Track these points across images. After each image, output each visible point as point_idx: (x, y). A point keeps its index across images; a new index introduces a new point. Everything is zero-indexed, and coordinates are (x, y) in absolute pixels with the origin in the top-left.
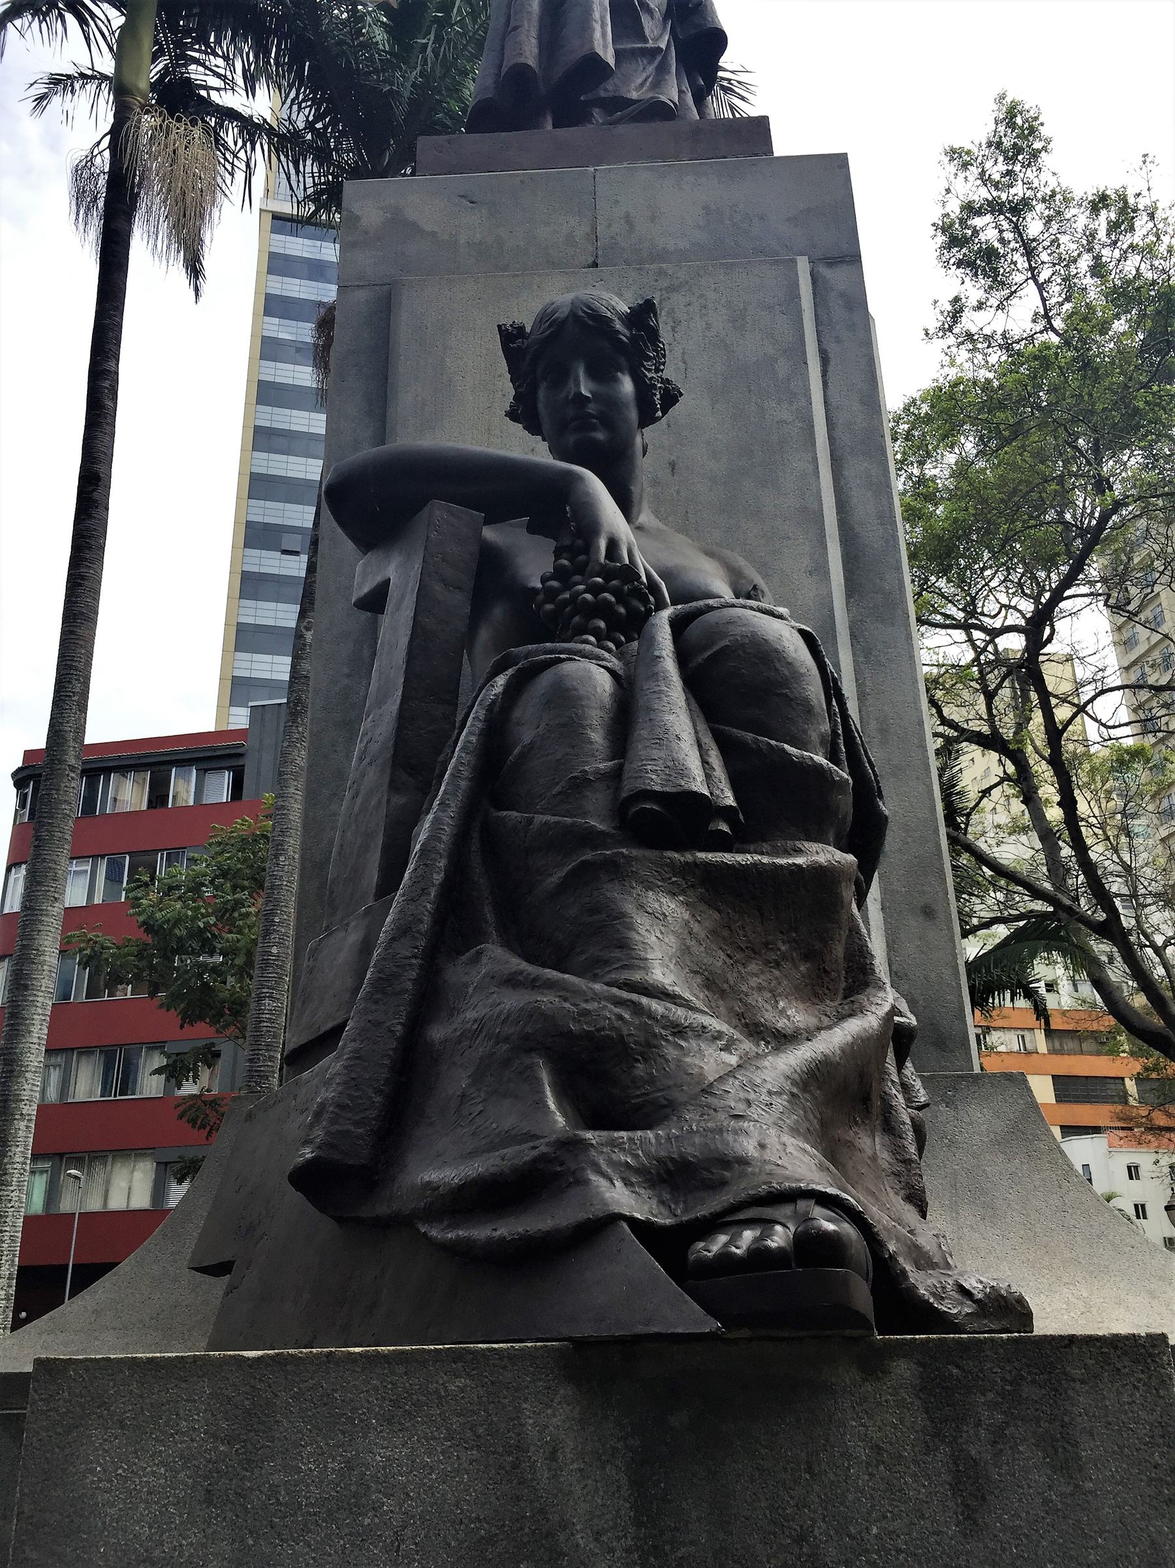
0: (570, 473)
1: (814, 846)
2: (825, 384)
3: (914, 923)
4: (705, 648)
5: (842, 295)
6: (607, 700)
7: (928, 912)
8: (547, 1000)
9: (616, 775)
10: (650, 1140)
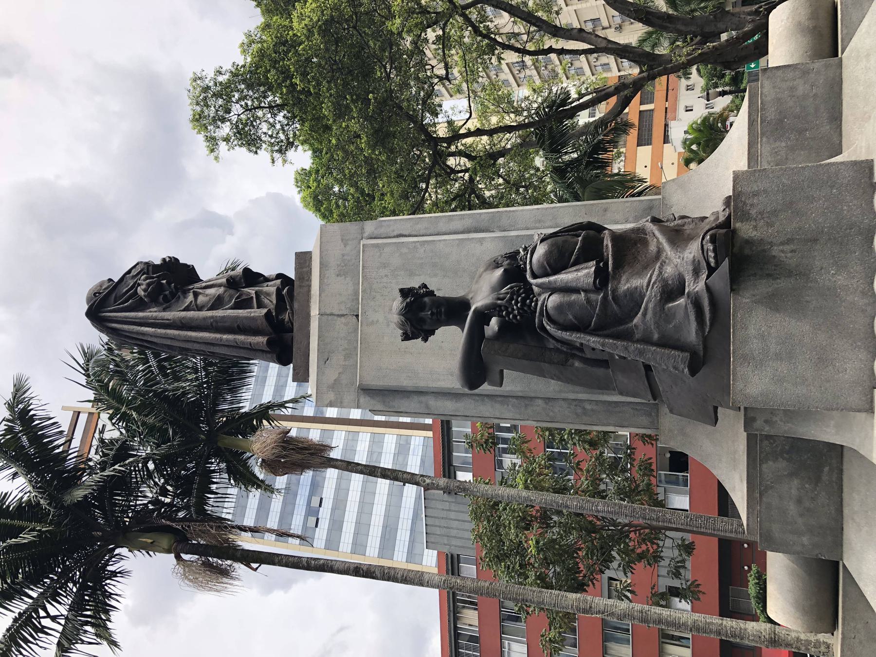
2: (410, 236)
3: (609, 214)
4: (546, 269)
6: (561, 295)
7: (605, 210)
8: (651, 305)
9: (585, 291)
10: (688, 278)
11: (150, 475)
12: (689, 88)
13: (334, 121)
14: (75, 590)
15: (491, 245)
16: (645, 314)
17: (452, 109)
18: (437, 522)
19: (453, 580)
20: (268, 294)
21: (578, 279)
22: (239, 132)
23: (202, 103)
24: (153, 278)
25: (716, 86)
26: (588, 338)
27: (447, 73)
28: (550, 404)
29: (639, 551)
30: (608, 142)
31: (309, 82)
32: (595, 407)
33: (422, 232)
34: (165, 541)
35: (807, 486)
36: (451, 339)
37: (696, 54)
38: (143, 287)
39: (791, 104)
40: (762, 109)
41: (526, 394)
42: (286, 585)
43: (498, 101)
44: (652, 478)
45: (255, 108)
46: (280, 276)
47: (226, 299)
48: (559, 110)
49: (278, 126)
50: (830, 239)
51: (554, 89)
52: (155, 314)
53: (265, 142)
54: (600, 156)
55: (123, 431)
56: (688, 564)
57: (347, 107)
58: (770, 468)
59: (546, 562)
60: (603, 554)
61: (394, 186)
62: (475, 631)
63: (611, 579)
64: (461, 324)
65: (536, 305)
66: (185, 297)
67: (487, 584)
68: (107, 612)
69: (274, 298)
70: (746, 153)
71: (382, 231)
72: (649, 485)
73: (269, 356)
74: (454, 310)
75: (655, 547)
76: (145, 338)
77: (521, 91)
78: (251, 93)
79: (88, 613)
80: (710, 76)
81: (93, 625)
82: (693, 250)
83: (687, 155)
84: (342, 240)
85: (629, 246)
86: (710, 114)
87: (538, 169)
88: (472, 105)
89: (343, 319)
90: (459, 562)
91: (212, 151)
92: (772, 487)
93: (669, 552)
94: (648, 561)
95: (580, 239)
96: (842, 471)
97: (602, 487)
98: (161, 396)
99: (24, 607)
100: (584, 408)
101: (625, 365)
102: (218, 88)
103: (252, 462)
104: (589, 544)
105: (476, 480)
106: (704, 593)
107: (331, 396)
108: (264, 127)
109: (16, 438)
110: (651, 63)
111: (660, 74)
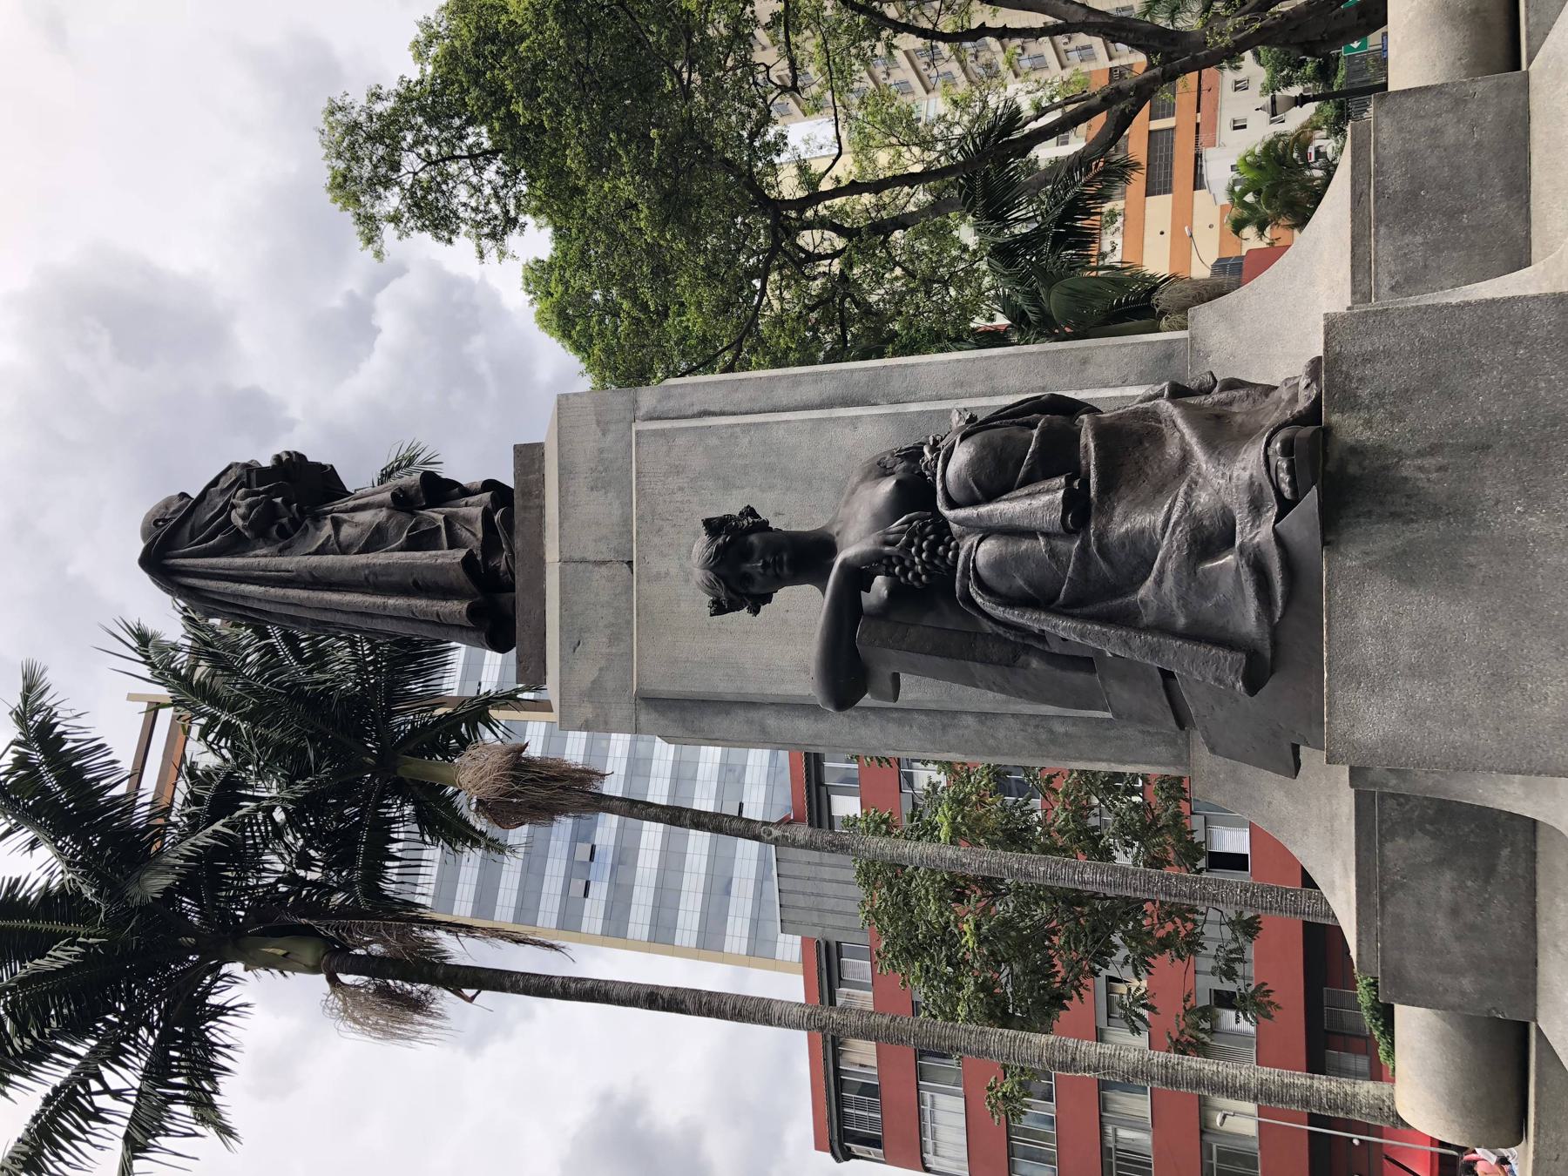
0: (842, 566)
1: (1083, 441)
2: (722, 414)
3: (1091, 370)
5: (659, 401)
6: (1002, 541)
7: (1085, 362)
8: (1170, 566)
9: (1046, 535)
10: (1241, 516)
11: (278, 832)
12: (1239, 86)
13: (589, 179)
14: (151, 1041)
15: (871, 431)
16: (1159, 582)
17: (806, 142)
18: (800, 886)
19: (826, 1014)
20: (468, 520)
21: (1032, 513)
22: (417, 205)
23: (348, 155)
24: (257, 494)
25: (1288, 83)
26: (1054, 621)
27: (795, 78)
28: (989, 723)
29: (1161, 933)
30: (1092, 197)
31: (540, 108)
32: (1071, 729)
33: (745, 406)
34: (307, 953)
35: (1469, 883)
36: (802, 609)
37: (1251, 30)
38: (241, 511)
39: (1432, 161)
40: (1376, 171)
41: (938, 737)
42: (528, 1015)
43: (889, 125)
44: (1182, 803)
45: (444, 160)
46: (489, 485)
47: (392, 532)
48: (1001, 140)
49: (488, 190)
50: (1513, 446)
51: (992, 101)
52: (263, 561)
53: (464, 221)
54: (1079, 224)
55: (228, 756)
56: (1250, 952)
57: (613, 151)
58: (1400, 850)
59: (994, 960)
60: (1096, 942)
61: (704, 292)
62: (871, 1075)
63: (1111, 979)
64: (821, 582)
65: (956, 556)
66: (318, 529)
67: (886, 1021)
68: (211, 1078)
69: (478, 527)
70: (1349, 256)
71: (671, 405)
72: (1177, 816)
73: (473, 635)
74: (807, 555)
75: (1189, 926)
76: (249, 604)
77: (932, 102)
78: (436, 132)
79: (180, 1080)
80: (1277, 68)
81: (187, 1100)
82: (1248, 463)
83: (1236, 212)
84: (598, 422)
85: (1129, 445)
86: (1279, 136)
87: (965, 248)
88: (844, 135)
89: (604, 570)
90: (840, 956)
91: (370, 241)
92: (1402, 886)
93: (1215, 934)
94: (1177, 951)
95: (1035, 432)
96: (1534, 854)
97: (1093, 822)
98: (295, 692)
99: (67, 1072)
100: (1051, 731)
101: (1126, 671)
102: (376, 125)
103: (461, 800)
104: (1071, 925)
105: (867, 814)
106: (1278, 1007)
107: (587, 711)
108: (462, 193)
109: (34, 770)
110: (1167, 49)
111: (1185, 70)
